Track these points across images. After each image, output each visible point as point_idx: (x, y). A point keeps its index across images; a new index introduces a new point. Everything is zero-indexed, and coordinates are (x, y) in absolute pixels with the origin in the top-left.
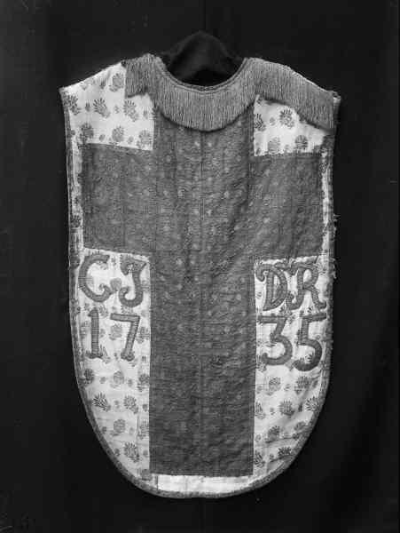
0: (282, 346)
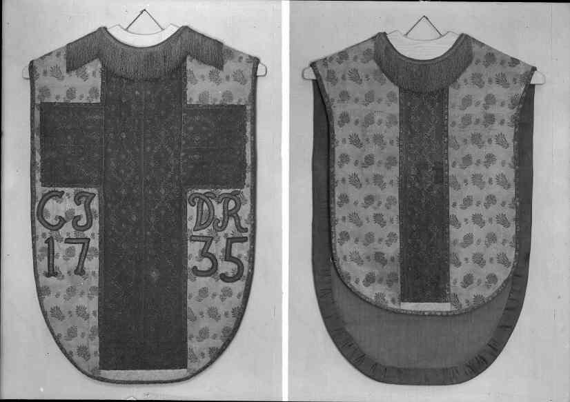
0: (210, 262)
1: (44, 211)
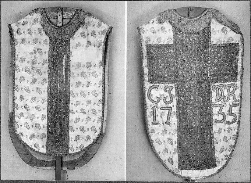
0: (222, 116)
1: (150, 95)
